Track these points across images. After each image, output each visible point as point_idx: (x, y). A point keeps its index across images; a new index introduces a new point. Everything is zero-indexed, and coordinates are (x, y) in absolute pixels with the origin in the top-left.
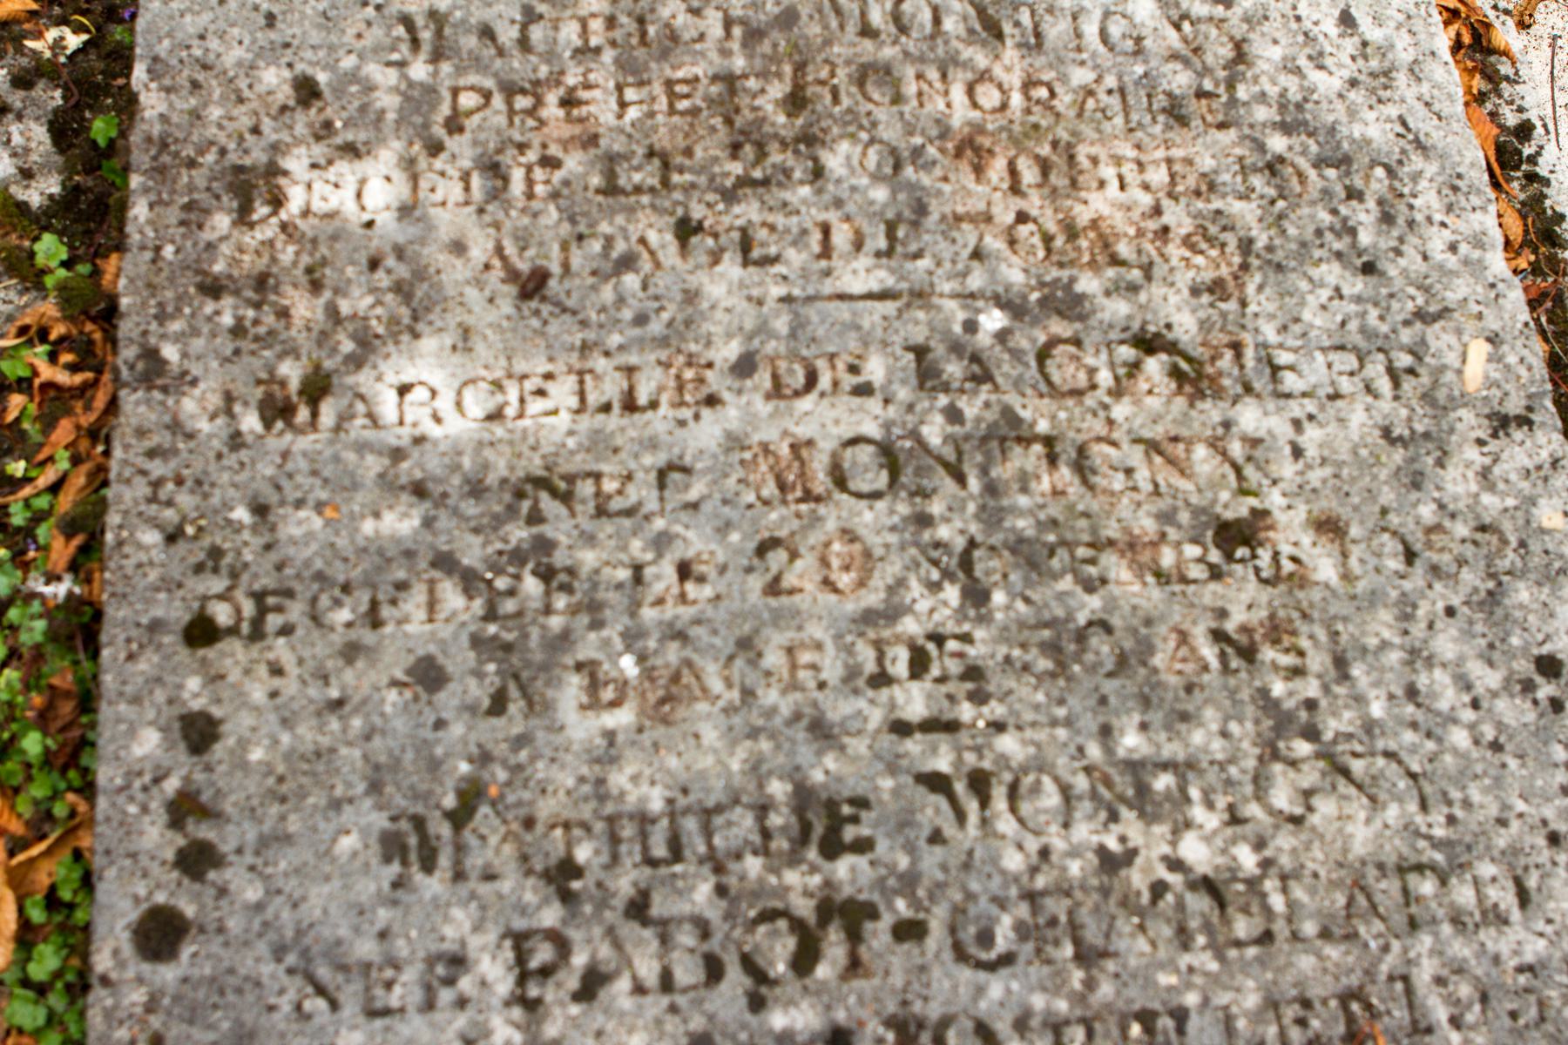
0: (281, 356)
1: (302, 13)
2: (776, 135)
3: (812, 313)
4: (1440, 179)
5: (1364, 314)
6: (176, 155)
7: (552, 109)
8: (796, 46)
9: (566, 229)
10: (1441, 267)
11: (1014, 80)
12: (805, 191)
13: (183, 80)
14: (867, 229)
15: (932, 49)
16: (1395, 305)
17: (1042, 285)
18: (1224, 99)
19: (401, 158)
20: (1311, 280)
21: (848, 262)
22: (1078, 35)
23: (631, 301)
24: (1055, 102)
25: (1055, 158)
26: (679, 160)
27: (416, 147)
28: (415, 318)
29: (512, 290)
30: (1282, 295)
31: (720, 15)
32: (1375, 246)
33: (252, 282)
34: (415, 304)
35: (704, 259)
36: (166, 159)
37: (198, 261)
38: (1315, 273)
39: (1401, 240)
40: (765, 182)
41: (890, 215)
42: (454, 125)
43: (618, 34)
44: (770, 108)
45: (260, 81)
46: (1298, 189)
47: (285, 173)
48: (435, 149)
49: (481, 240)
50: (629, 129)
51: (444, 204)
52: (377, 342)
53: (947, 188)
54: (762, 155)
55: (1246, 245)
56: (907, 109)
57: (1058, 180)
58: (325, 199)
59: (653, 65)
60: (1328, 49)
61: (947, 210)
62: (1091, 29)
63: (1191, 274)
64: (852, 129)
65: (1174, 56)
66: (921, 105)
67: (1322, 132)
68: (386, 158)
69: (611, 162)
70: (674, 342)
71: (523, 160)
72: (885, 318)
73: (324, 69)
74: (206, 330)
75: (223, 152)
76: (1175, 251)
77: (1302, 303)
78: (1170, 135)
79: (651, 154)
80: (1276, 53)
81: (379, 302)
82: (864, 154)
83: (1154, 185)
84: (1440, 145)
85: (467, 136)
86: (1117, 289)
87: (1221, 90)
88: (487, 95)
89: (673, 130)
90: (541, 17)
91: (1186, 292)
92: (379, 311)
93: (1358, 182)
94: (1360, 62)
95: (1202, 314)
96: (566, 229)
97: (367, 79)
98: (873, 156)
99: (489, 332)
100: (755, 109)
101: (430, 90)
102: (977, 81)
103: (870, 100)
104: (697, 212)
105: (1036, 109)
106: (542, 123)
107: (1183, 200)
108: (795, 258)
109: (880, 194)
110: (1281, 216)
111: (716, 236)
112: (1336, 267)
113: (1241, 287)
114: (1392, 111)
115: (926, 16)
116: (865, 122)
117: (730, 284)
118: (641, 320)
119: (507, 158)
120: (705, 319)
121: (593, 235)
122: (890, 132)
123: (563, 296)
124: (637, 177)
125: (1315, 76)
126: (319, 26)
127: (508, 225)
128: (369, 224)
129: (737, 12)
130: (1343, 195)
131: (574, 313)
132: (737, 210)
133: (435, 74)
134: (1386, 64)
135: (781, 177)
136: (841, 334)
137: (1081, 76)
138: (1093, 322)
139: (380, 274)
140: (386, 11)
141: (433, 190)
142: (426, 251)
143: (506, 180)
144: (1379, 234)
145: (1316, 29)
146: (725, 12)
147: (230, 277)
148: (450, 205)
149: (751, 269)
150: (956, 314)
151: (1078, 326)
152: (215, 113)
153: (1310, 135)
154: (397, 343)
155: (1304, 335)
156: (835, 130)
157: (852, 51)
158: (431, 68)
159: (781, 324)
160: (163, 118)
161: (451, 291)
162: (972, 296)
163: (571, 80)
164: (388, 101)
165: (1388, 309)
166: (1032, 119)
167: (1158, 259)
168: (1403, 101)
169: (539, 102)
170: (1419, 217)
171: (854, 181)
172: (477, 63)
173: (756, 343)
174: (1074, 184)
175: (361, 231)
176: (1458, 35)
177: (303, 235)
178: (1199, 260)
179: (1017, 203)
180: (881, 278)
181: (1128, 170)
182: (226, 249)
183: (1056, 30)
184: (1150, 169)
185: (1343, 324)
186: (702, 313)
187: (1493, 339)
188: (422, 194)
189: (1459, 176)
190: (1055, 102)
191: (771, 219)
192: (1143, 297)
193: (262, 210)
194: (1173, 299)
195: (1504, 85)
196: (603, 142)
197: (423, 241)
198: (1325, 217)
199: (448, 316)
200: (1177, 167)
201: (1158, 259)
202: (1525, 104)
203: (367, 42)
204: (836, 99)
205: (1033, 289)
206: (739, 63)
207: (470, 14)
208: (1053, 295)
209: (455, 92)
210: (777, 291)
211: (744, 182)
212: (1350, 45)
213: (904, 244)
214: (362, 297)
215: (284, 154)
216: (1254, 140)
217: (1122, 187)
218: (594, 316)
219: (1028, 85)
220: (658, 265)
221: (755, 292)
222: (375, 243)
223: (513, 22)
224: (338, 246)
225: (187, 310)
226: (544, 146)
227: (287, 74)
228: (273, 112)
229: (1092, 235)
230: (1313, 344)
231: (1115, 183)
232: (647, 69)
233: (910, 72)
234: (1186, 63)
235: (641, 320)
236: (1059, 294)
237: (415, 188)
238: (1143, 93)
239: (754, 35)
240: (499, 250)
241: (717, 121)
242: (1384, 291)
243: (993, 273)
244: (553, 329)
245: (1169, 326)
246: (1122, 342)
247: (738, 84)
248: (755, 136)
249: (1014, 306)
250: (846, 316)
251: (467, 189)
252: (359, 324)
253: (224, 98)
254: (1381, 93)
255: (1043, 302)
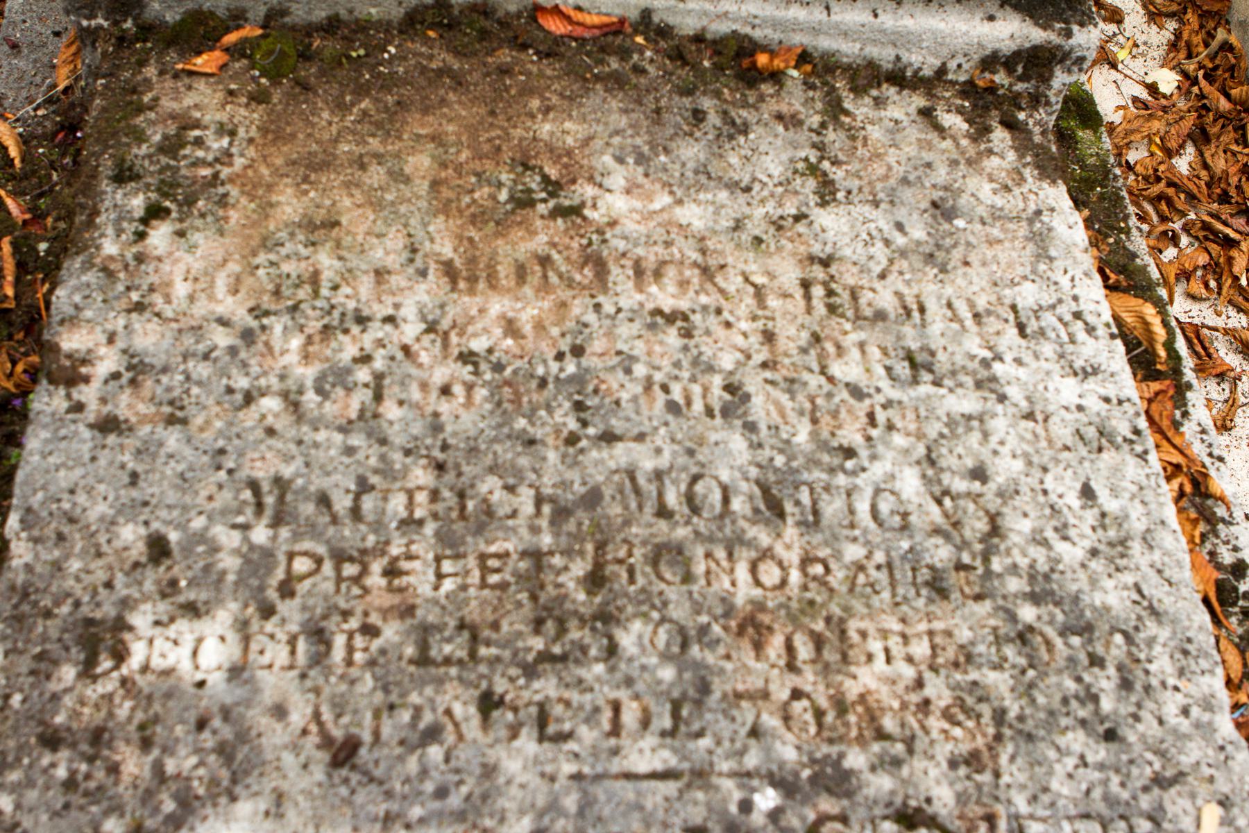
0: (107, 813)
1: (162, 473)
2: (576, 613)
3: (599, 791)
4: (1172, 644)
5: (1105, 782)
6: (35, 604)
7: (376, 580)
8: (598, 525)
9: (379, 697)
10: (1175, 731)
11: (793, 557)
12: (599, 668)
13: (50, 531)
14: (653, 708)
15: (720, 529)
16: (1135, 771)
17: (813, 761)
18: (980, 571)
19: (236, 620)
20: (1058, 749)
21: (635, 741)
22: (852, 512)
23: (434, 774)
24: (830, 578)
25: (828, 634)
26: (486, 633)
27: (251, 610)
28: (234, 781)
29: (324, 756)
30: (1031, 765)
31: (532, 492)
32: (1115, 712)
33: (87, 735)
34: (235, 766)
35: (503, 733)
36: (25, 608)
37: (42, 711)
38: (1062, 741)
39: (1139, 705)
40: (563, 658)
41: (676, 694)
42: (287, 590)
43: (440, 507)
44: (571, 585)
45: (118, 536)
46: (1046, 657)
47: (131, 629)
48: (267, 611)
49: (301, 705)
50: (443, 601)
51: (270, 666)
52: (197, 804)
53: (729, 666)
54: (562, 630)
55: (1000, 716)
56: (695, 588)
57: (830, 655)
58: (163, 656)
59: (469, 539)
60: (1072, 521)
61: (728, 688)
62: (863, 507)
63: (949, 746)
64: (645, 608)
65: (937, 531)
66: (709, 584)
67: (1067, 601)
68: (223, 619)
69: (424, 633)
70: (471, 817)
71: (345, 626)
72: (667, 799)
73: (176, 528)
74: (40, 782)
75: (77, 604)
76: (936, 723)
77: (1050, 773)
78: (932, 608)
79: (462, 626)
80: (1026, 526)
81: (201, 764)
82: (655, 632)
83: (917, 658)
84: (1172, 610)
85: (297, 601)
86: (882, 763)
87: (978, 562)
88: (319, 561)
89: (484, 603)
90: (373, 488)
91: (944, 765)
92: (201, 772)
93: (1099, 649)
94: (1100, 532)
95: (959, 787)
96: (379, 697)
97: (213, 540)
98: (662, 636)
99: (300, 798)
100: (559, 586)
101: (268, 554)
102: (760, 559)
103: (662, 579)
104: (500, 686)
105: (812, 585)
106: (366, 591)
107: (943, 672)
108: (587, 735)
109: (667, 673)
110: (1031, 685)
111: (515, 710)
112: (1080, 735)
113: (995, 757)
114: (1129, 578)
115: (717, 496)
116: (657, 602)
117: (526, 760)
118: (442, 793)
119: (332, 624)
120: (500, 794)
121: (404, 705)
122: (680, 611)
123: (371, 766)
124: (447, 649)
125: (1061, 547)
126: (176, 487)
127: (327, 691)
128: (201, 684)
129: (547, 491)
130: (1086, 662)
131: (381, 783)
132: (536, 685)
133: (274, 538)
134: (1123, 534)
135: (578, 654)
136: (625, 815)
137: (854, 552)
138: (859, 798)
139: (206, 734)
140: (237, 475)
141: (262, 652)
142: (250, 713)
143: (329, 645)
144: (1119, 700)
145: (1061, 502)
146: (537, 489)
147: (69, 729)
148: (276, 668)
149: (546, 745)
150: (731, 791)
151: (845, 802)
152: (75, 565)
153: (1057, 604)
154: (215, 805)
155: (1053, 804)
156: (630, 609)
157: (647, 532)
158: (270, 532)
159: (570, 802)
160: (28, 568)
161: (269, 756)
162: (748, 775)
163: (395, 550)
164: (229, 563)
165: (1128, 775)
166: (808, 595)
167: (919, 733)
168: (1138, 569)
169: (365, 571)
170: (1155, 682)
171: (644, 660)
172: (313, 530)
173: (546, 820)
174: (845, 658)
175: (192, 690)
176: (1181, 486)
177: (140, 691)
178: (957, 732)
179: (792, 680)
180: (664, 758)
181: (894, 643)
182: (68, 701)
183: (832, 508)
184: (914, 641)
185: (1088, 792)
186: (498, 788)
187: (1224, 803)
188: (252, 656)
189: (1189, 640)
190: (830, 578)
191: (566, 694)
192: (905, 771)
193: (106, 664)
194: (933, 772)
195: (1221, 526)
196: (419, 613)
197: (248, 703)
198: (1071, 685)
199: (265, 780)
200: (938, 640)
201: (919, 733)
202: (1240, 544)
203: (217, 504)
204: (632, 580)
205: (804, 766)
206: (546, 540)
207: (309, 482)
208: (823, 771)
209: (291, 556)
210: (568, 768)
211: (545, 657)
212: (1091, 516)
213: (687, 724)
214: (187, 757)
215: (132, 609)
216: (1007, 611)
217: (889, 660)
218: (398, 786)
219: (806, 561)
220: (461, 737)
221: (549, 769)
222: (204, 703)
223: (348, 491)
224: (171, 704)
225: (26, 761)
226: (366, 614)
227: (142, 531)
228: (127, 567)
229: (860, 709)
230: (1061, 813)
231: (881, 657)
232: (464, 543)
233: (700, 551)
234: (947, 537)
235: (442, 793)
236: (829, 770)
237: (246, 649)
238: (908, 567)
239: (561, 514)
240: (317, 715)
241: (523, 596)
242: (1124, 757)
243: (768, 751)
244: (360, 798)
245: (929, 800)
246: (885, 818)
247: (545, 560)
248: (557, 613)
249: (785, 784)
250: (631, 796)
251: (293, 652)
252: (182, 784)
253: (84, 551)
254: (1119, 561)
255: (813, 780)
